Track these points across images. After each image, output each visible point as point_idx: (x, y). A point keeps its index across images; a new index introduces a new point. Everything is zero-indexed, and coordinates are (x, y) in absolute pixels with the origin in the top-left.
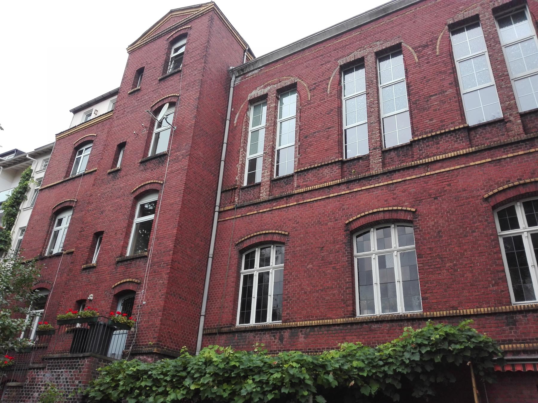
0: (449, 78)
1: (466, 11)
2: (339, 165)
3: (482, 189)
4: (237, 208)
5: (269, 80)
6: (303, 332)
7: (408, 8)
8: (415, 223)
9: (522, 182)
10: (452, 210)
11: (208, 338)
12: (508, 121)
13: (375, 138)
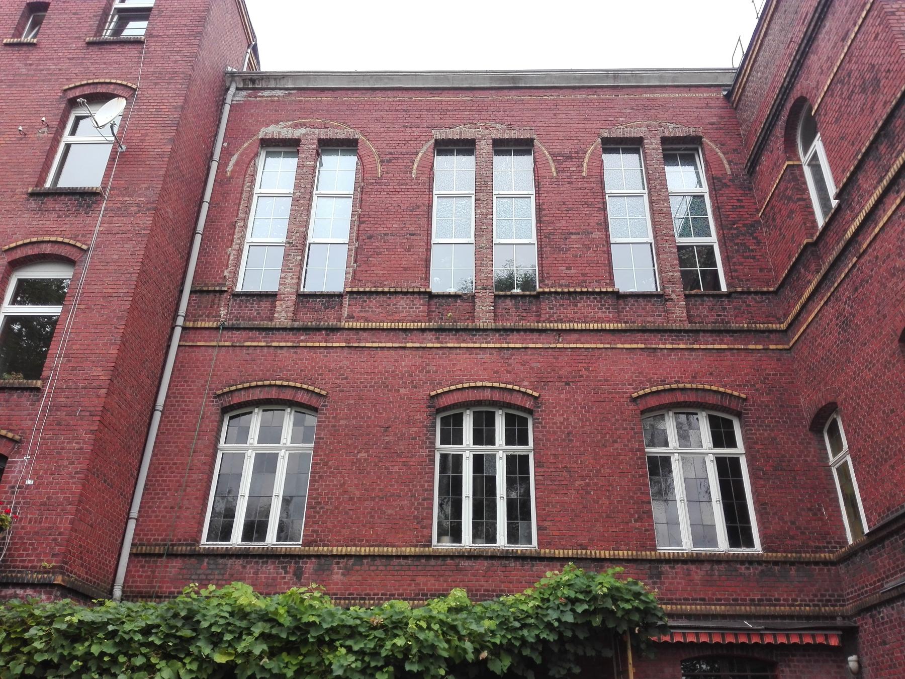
0: (598, 215)
1: (627, 127)
2: (425, 298)
3: (630, 385)
4: (225, 329)
5: (305, 118)
6: (341, 565)
7: (548, 91)
8: (536, 414)
9: (681, 386)
10: (589, 406)
11: (139, 562)
12: (669, 299)
13: (486, 273)
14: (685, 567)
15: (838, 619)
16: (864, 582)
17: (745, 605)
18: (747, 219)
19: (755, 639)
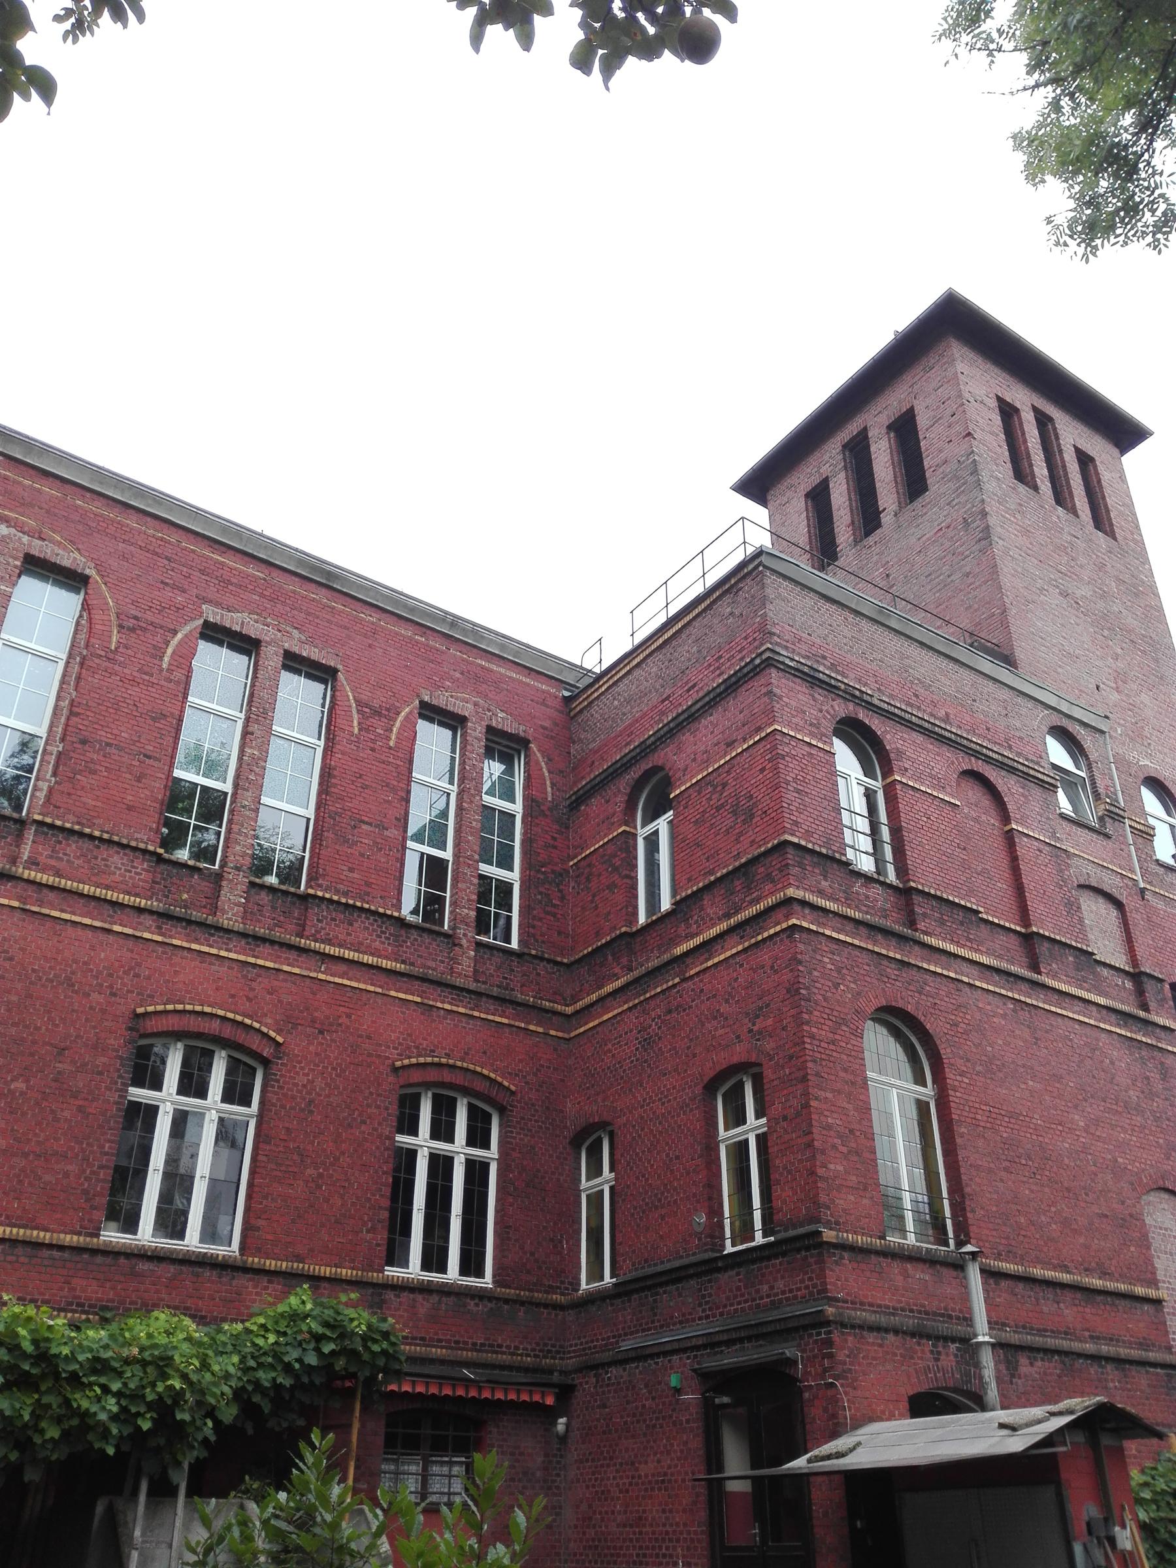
5: (11, 510)
9: (451, 1062)
14: (411, 1296)
15: (556, 1374)
16: (595, 1335)
17: (467, 1350)
18: (556, 864)
19: (473, 1393)
